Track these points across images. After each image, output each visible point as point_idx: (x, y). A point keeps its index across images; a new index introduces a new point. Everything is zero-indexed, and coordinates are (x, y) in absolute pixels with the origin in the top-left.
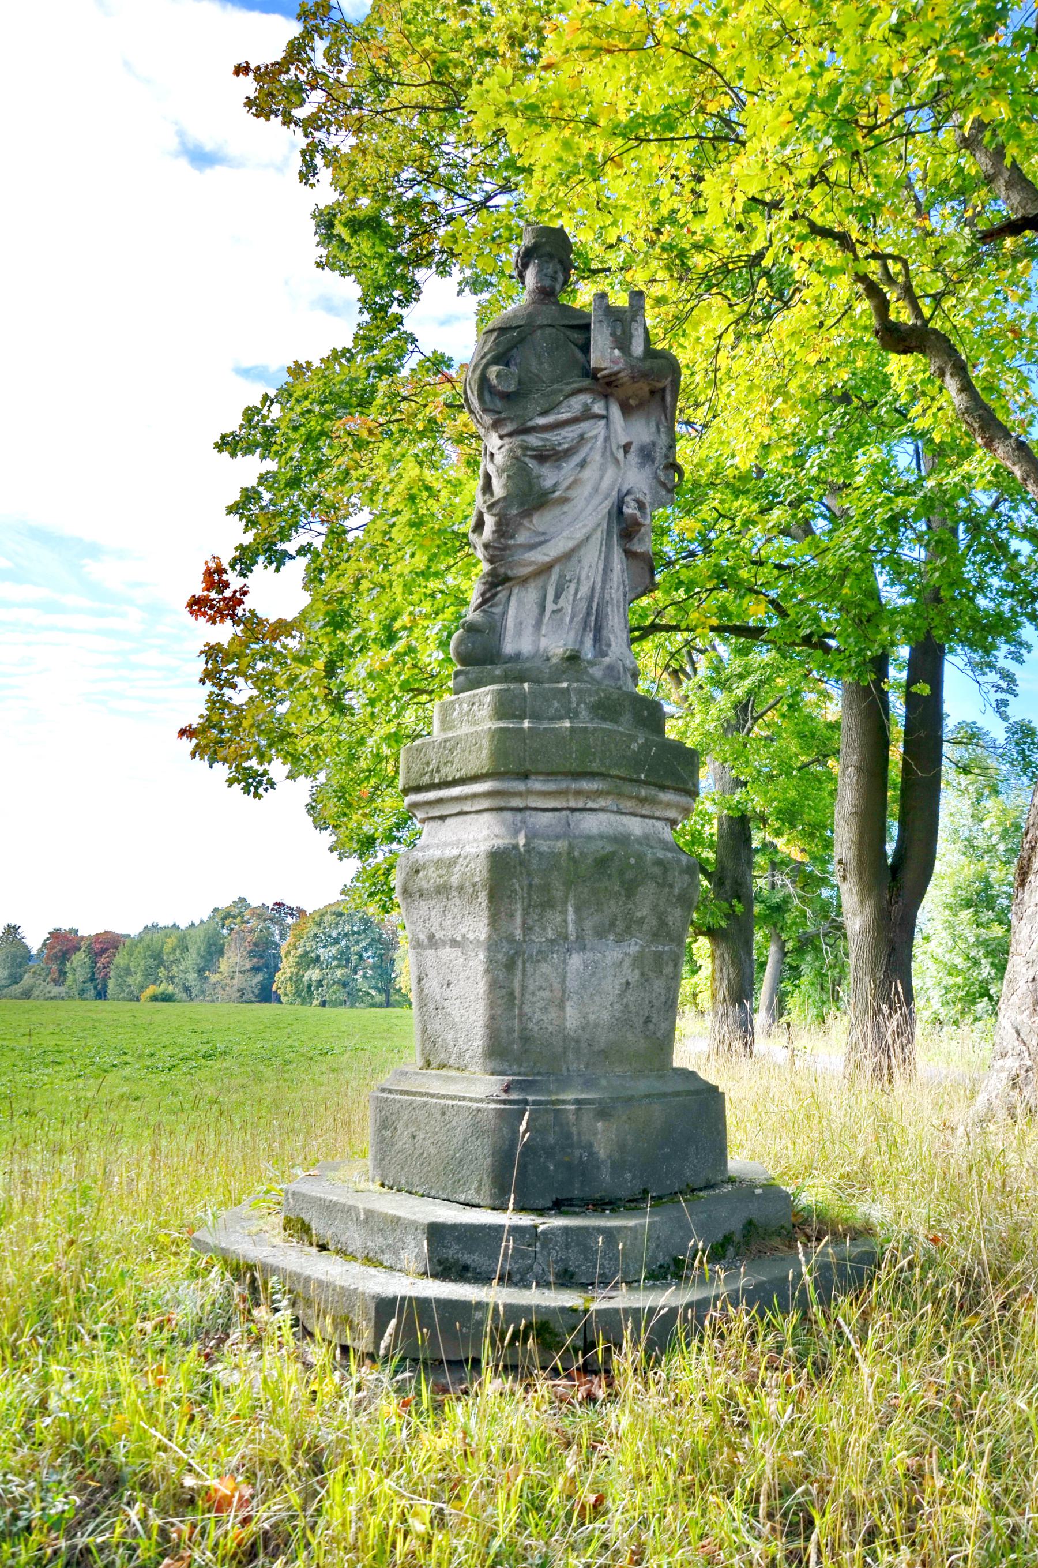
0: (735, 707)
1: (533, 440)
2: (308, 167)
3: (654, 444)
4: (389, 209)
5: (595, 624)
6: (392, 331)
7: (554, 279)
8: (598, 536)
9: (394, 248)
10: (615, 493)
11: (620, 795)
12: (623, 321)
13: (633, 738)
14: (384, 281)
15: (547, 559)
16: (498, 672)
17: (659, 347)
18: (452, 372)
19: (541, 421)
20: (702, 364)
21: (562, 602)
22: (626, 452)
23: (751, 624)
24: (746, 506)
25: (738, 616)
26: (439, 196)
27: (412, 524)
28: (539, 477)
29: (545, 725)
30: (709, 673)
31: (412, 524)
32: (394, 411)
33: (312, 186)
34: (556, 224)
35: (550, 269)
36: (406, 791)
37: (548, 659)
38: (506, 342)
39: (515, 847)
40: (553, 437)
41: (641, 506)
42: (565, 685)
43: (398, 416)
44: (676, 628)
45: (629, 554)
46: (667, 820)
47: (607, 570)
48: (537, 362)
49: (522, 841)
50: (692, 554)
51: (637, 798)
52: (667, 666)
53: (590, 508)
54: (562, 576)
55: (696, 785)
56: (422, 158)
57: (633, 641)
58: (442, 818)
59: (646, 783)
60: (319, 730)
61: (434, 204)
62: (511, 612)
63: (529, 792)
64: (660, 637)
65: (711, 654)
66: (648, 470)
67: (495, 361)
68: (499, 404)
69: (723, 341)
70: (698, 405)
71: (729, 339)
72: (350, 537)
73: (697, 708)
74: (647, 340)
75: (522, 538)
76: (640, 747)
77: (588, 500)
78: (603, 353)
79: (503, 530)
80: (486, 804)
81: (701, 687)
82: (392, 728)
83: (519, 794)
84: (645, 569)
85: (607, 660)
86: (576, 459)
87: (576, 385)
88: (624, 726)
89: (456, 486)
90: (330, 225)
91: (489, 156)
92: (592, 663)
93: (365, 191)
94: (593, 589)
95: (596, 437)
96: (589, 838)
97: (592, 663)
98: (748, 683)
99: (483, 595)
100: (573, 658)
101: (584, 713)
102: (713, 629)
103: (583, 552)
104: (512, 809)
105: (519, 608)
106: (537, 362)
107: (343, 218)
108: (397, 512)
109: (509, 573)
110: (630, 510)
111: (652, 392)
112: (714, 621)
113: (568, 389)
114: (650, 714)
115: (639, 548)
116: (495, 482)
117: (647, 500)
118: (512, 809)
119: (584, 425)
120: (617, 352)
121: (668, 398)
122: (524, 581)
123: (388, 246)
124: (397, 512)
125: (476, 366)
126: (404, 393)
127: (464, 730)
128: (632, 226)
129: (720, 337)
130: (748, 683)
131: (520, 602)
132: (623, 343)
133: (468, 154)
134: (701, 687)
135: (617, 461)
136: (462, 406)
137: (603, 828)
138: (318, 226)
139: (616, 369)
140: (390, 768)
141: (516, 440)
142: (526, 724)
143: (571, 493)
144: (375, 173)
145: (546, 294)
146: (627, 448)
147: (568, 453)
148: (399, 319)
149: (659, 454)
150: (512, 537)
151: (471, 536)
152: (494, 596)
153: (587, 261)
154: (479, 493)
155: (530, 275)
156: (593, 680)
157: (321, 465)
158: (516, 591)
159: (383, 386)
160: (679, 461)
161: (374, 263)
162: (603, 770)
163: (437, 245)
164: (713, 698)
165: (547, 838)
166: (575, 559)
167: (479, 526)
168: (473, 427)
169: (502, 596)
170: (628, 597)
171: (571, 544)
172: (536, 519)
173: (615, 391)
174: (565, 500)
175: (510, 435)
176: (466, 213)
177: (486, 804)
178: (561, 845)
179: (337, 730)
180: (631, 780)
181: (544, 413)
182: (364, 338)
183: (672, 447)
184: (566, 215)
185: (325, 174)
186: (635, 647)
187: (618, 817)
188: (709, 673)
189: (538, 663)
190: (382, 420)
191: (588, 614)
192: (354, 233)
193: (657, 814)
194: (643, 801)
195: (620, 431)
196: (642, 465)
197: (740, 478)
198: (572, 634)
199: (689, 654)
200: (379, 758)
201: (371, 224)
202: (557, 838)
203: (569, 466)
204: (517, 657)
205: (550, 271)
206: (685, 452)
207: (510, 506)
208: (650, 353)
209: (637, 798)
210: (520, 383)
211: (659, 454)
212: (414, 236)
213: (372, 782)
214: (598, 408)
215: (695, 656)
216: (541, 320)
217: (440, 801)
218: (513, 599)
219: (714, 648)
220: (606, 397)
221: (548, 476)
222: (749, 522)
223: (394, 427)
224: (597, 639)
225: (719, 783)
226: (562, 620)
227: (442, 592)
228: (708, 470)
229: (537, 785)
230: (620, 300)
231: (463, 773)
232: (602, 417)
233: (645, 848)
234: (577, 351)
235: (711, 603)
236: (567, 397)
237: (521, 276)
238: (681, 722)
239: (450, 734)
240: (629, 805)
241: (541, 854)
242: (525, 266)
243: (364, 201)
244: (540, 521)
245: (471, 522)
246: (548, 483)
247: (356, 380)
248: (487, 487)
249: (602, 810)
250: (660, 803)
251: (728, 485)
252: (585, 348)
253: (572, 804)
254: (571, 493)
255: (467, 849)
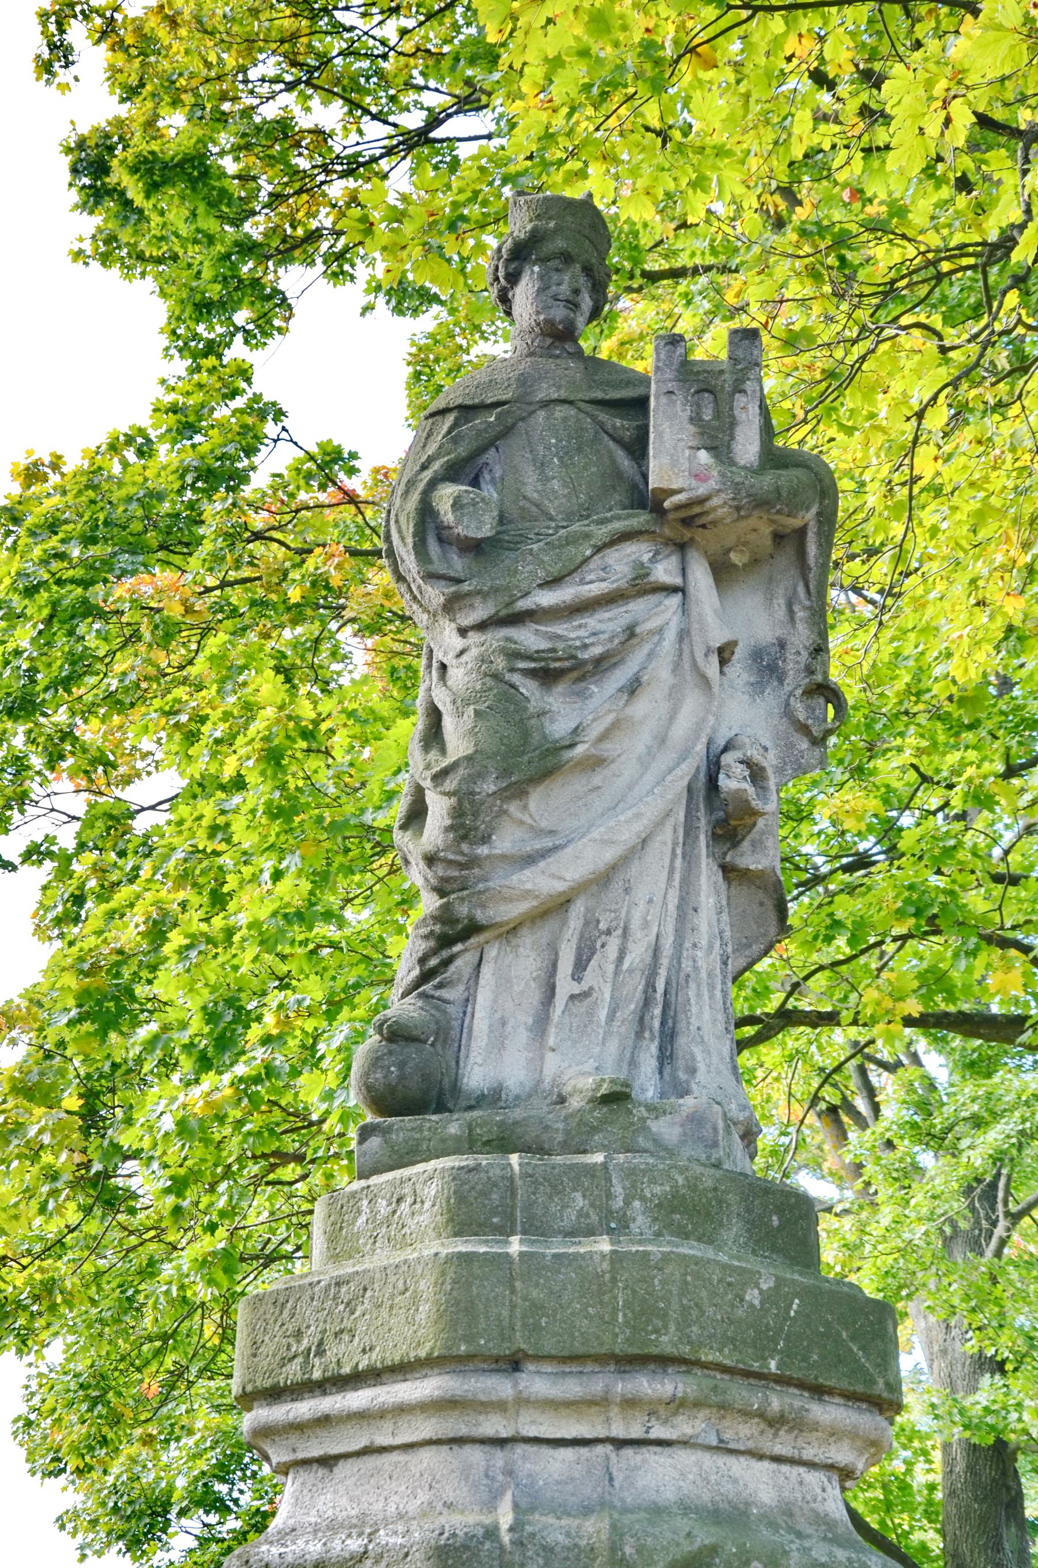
0: (968, 1191)
1: (529, 638)
2: (52, 47)
3: (782, 645)
4: (225, 139)
5: (662, 1025)
6: (234, 393)
7: (573, 305)
8: (666, 835)
9: (237, 222)
10: (700, 747)
11: (724, 1408)
12: (715, 391)
13: (749, 1278)
14: (214, 292)
15: (560, 886)
16: (453, 1129)
17: (792, 441)
18: (354, 484)
19: (546, 598)
20: (879, 470)
21: (591, 977)
22: (723, 662)
23: (995, 1009)
24: (976, 763)
25: (967, 988)
26: (327, 114)
27: (275, 813)
28: (542, 714)
29: (557, 1247)
30: (907, 1114)
31: (275, 813)
32: (238, 565)
33: (64, 87)
34: (575, 192)
35: (565, 283)
36: (247, 1399)
37: (562, 1100)
38: (468, 432)
39: (491, 1533)
40: (572, 632)
41: (756, 774)
42: (599, 1158)
43: (246, 572)
44: (830, 1019)
45: (728, 871)
46: (831, 1467)
47: (686, 909)
48: (539, 473)
49: (505, 1518)
50: (863, 862)
51: (761, 1415)
52: (815, 1099)
53: (649, 778)
54: (590, 921)
55: (894, 1387)
56: (293, 37)
57: (742, 1045)
58: (327, 1462)
59: (782, 1380)
60: (56, 1247)
61: (320, 135)
62: (483, 997)
63: (522, 1402)
64: (796, 1037)
65: (911, 1073)
66: (771, 700)
67: (452, 473)
68: (458, 564)
69: (926, 423)
70: (872, 552)
71: (938, 418)
72: (141, 824)
73: (885, 1191)
74: (768, 431)
75: (506, 840)
76: (767, 1298)
77: (645, 763)
78: (675, 461)
79: (466, 826)
80: (425, 1428)
81: (890, 1145)
82: (219, 1241)
83: (500, 1406)
84: (765, 904)
85: (688, 1103)
86: (620, 677)
87: (618, 525)
88: (727, 1251)
89: (367, 724)
90: (100, 168)
91: (433, 36)
92: (655, 1110)
93: (176, 103)
94: (656, 952)
95: (660, 631)
96: (657, 1511)
97: (655, 1110)
98: (994, 1136)
99: (422, 961)
100: (616, 1098)
101: (641, 1222)
102: (909, 1022)
103: (634, 869)
104: (483, 1441)
105: (498, 989)
106: (539, 473)
107: (130, 155)
108: (239, 784)
109: (480, 916)
110: (733, 781)
111: (778, 538)
112: (914, 1007)
113: (602, 533)
114: (780, 1211)
115: (748, 859)
116: (448, 723)
117: (770, 761)
118: (483, 1441)
119: (637, 607)
120: (703, 456)
121: (812, 549)
122: (512, 931)
123: (222, 218)
124: (239, 784)
125: (411, 484)
126: (258, 521)
127: (381, 1258)
128: (727, 200)
129: (920, 415)
130: (994, 1136)
131: (504, 982)
132: (717, 438)
133: (390, 30)
134: (890, 1145)
135: (705, 682)
136: (377, 553)
137: (687, 1488)
138: (75, 171)
139: (702, 490)
140: (209, 1329)
141: (495, 637)
142: (515, 1246)
143: (609, 748)
144: (196, 65)
145: (558, 336)
146: (724, 654)
147: (602, 664)
148: (245, 373)
149: (794, 664)
150: (485, 839)
151: (398, 836)
152: (447, 962)
153: (635, 250)
154: (416, 747)
155: (524, 295)
156: (660, 1146)
157: (80, 666)
158: (492, 952)
159: (214, 509)
160: (835, 674)
161: (194, 253)
162: (686, 1350)
163: (325, 219)
164: (918, 1170)
165: (561, 1510)
166: (617, 886)
167: (416, 815)
168: (402, 603)
169: (462, 965)
170: (736, 963)
171: (609, 855)
172: (535, 799)
173: (699, 535)
174: (595, 763)
175: (482, 626)
176: (389, 152)
177: (425, 1428)
178: (594, 1529)
179: (95, 1246)
180: (748, 1374)
181: (553, 582)
182: (174, 409)
183: (820, 650)
184: (595, 169)
185: (92, 58)
186: (746, 1059)
187: (722, 1461)
188: (907, 1114)
189: (540, 1108)
190: (211, 582)
191: (647, 1002)
192: (152, 188)
193: (808, 1454)
194: (775, 1422)
195: (710, 618)
196: (757, 688)
197: (963, 702)
198: (613, 1046)
199: (862, 1071)
200: (186, 1306)
201: (192, 171)
202: (586, 1511)
203: (604, 690)
204: (492, 1098)
205: (564, 290)
206: (851, 653)
207: (480, 776)
208: (774, 458)
209: (761, 1415)
210: (502, 519)
211: (794, 664)
212: (276, 198)
213: (169, 1361)
214: (664, 572)
215: (878, 1078)
216: (545, 391)
217: (324, 1421)
218: (487, 971)
219: (915, 1059)
220: (682, 547)
221: (561, 713)
222: (983, 800)
223: (237, 596)
224: (666, 1057)
225: (940, 1364)
226: (591, 1014)
227: (334, 945)
228: (900, 685)
229: (537, 1383)
230: (712, 346)
231: (374, 1358)
232: (674, 590)
233: (784, 1537)
234: (620, 454)
235: (910, 962)
236: (598, 550)
237: (505, 299)
238: (848, 1222)
239: (348, 1268)
240: (743, 1432)
241: (548, 1550)
242: (513, 278)
243: (175, 122)
244: (543, 806)
245: (399, 808)
246: (559, 728)
247: (160, 497)
248: (433, 734)
249: (684, 1443)
250: (815, 1427)
251: (937, 715)
252: (638, 448)
253: (618, 1430)
254: (609, 748)
255: (383, 1537)
